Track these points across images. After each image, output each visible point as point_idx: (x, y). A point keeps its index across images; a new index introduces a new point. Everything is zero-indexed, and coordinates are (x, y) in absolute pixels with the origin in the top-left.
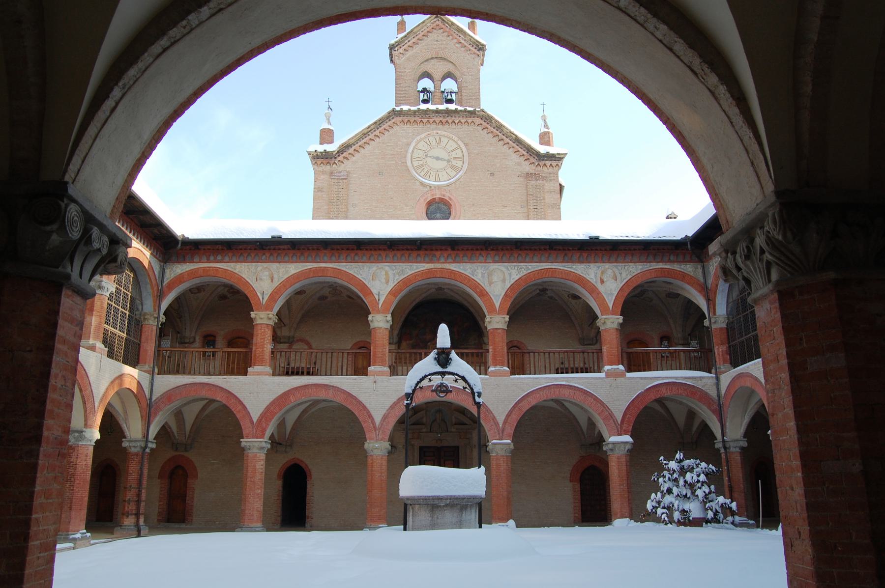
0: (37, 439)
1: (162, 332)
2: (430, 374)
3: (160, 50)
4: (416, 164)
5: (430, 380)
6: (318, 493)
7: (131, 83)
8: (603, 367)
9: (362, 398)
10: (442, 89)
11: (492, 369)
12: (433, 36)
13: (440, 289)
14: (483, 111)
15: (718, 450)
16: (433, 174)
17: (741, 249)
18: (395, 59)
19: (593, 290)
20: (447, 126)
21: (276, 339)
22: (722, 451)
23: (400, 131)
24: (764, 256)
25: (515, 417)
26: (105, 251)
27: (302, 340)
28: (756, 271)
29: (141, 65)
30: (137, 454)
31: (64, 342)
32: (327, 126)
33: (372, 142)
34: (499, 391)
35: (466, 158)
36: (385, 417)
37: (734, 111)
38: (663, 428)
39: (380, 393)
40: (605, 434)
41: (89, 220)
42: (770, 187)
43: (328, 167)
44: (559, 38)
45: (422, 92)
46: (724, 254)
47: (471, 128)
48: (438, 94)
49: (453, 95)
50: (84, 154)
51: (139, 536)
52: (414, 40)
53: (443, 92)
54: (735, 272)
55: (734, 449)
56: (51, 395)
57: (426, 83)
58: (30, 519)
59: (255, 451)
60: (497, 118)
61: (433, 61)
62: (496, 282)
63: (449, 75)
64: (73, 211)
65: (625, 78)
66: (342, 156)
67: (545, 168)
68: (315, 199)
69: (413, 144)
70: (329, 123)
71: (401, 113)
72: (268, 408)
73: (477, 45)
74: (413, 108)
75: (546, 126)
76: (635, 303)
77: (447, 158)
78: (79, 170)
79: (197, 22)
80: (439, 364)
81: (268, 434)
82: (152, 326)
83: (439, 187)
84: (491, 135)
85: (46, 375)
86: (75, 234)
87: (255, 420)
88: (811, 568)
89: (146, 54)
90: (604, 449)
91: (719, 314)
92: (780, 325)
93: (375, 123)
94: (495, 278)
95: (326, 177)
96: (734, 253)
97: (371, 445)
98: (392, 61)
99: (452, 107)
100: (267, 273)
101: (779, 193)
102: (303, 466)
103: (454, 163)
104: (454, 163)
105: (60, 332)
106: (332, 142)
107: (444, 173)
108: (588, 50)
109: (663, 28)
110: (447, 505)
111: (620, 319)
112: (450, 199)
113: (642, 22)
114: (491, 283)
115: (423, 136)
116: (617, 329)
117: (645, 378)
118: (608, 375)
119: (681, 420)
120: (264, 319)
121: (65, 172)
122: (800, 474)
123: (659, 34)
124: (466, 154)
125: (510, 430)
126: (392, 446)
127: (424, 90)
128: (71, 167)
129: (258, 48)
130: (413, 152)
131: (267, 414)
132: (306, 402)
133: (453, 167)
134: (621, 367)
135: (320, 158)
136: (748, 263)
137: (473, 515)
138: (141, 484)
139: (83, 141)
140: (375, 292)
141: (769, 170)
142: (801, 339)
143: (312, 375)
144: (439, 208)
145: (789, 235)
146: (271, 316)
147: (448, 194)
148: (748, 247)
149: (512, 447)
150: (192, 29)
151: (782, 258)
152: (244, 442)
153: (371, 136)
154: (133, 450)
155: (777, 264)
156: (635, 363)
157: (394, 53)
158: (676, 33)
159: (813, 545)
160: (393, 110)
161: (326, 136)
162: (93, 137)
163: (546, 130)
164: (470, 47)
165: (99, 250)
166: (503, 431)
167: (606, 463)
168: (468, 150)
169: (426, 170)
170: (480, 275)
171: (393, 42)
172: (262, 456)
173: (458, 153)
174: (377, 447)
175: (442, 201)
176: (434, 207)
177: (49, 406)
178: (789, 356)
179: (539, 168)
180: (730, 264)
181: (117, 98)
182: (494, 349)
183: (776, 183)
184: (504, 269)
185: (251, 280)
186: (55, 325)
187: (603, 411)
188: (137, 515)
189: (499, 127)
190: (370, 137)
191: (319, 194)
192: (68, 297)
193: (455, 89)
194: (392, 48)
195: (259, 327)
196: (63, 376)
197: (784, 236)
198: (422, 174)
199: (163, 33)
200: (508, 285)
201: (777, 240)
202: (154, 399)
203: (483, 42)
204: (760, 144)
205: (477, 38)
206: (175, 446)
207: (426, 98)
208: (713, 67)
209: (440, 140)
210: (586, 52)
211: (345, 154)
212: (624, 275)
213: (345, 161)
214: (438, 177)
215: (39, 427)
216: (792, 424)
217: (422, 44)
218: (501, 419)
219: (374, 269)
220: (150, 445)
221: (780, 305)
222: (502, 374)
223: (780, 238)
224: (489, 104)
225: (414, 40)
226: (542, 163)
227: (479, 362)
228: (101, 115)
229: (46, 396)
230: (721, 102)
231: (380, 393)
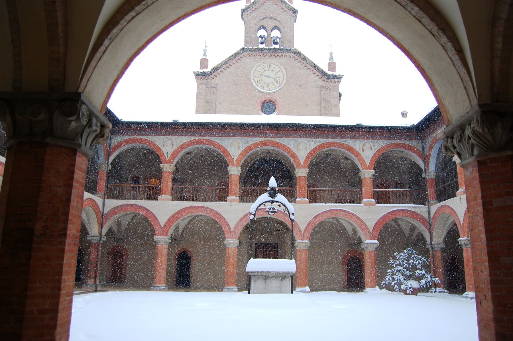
0: (65, 235)
1: (110, 175)
2: (265, 202)
3: (130, 18)
4: (256, 80)
5: (265, 205)
6: (196, 267)
7: (114, 37)
8: (362, 199)
9: (223, 214)
10: (272, 36)
11: (298, 200)
13: (269, 153)
14: (295, 49)
15: (428, 249)
16: (266, 85)
17: (456, 136)
18: (245, 18)
19: (357, 155)
20: (274, 58)
21: (174, 181)
22: (430, 249)
23: (247, 60)
24: (470, 141)
26: (98, 131)
28: (465, 149)
29: (120, 26)
30: (95, 244)
31: (78, 182)
33: (231, 67)
34: (302, 213)
35: (285, 77)
37: (456, 58)
38: (393, 236)
39: (235, 212)
40: (363, 238)
41: (91, 114)
42: (475, 102)
43: (205, 81)
44: (354, 13)
46: (446, 139)
49: (278, 39)
50: (88, 77)
51: (96, 291)
52: (255, 7)
54: (452, 149)
55: (437, 248)
56: (71, 211)
57: (262, 32)
58: (61, 279)
59: (162, 243)
62: (301, 151)
63: (276, 28)
64: (84, 110)
65: (392, 36)
66: (213, 74)
67: (331, 84)
68: (197, 99)
69: (254, 68)
72: (169, 220)
76: (382, 163)
77: (274, 77)
78: (86, 86)
79: (151, 2)
80: (270, 196)
81: (169, 234)
82: (104, 170)
83: (269, 93)
85: (69, 200)
86: (84, 122)
87: (162, 226)
88: (491, 316)
89: (123, 21)
90: (362, 247)
91: (431, 171)
92: (478, 180)
94: (301, 147)
96: (452, 138)
97: (228, 242)
98: (243, 19)
99: (277, 46)
100: (170, 142)
101: (481, 106)
103: (278, 79)
105: (76, 176)
108: (371, 20)
109: (417, 9)
110: (273, 277)
111: (373, 172)
113: (404, 5)
114: (298, 150)
115: (260, 63)
116: (371, 178)
117: (387, 207)
118: (365, 204)
119: (407, 232)
120: (168, 168)
121: (79, 87)
122: (487, 264)
123: (413, 12)
124: (285, 74)
125: (308, 235)
126: (240, 242)
127: (262, 37)
128: (82, 84)
129: (183, 16)
131: (170, 222)
132: (191, 216)
134: (373, 200)
135: (200, 76)
136: (460, 144)
137: (288, 283)
138: (97, 259)
139: (88, 70)
141: (475, 92)
142: (490, 188)
143: (195, 201)
144: (268, 106)
145: (486, 129)
146: (172, 166)
148: (461, 135)
150: (148, 6)
151: (481, 142)
152: (156, 238)
153: (230, 63)
154: (93, 241)
155: (477, 145)
156: (381, 198)
158: (424, 12)
159: (494, 303)
160: (243, 48)
161: (204, 62)
162: (94, 67)
164: (289, 11)
165: (96, 131)
167: (363, 255)
168: (286, 72)
169: (261, 84)
172: (166, 246)
174: (232, 242)
177: (70, 217)
178: (483, 197)
179: (327, 83)
180: (449, 145)
181: (106, 45)
183: (479, 99)
184: (306, 142)
185: (161, 146)
186: (73, 172)
187: (362, 225)
188: (95, 278)
189: (305, 59)
192: (80, 157)
194: (243, 11)
195: (165, 173)
196: (77, 201)
197: (483, 130)
198: (259, 86)
199: (132, 8)
201: (478, 132)
202: (105, 213)
204: (470, 77)
205: (292, 5)
206: (116, 240)
208: (444, 31)
210: (370, 21)
212: (376, 146)
213: (215, 77)
215: (65, 229)
216: (483, 236)
220: (103, 239)
221: (479, 169)
222: (304, 202)
223: (480, 131)
224: (298, 45)
225: (255, 7)
226: (329, 80)
227: (291, 196)
228: (98, 55)
229: (69, 212)
230: (448, 52)
231: (235, 212)
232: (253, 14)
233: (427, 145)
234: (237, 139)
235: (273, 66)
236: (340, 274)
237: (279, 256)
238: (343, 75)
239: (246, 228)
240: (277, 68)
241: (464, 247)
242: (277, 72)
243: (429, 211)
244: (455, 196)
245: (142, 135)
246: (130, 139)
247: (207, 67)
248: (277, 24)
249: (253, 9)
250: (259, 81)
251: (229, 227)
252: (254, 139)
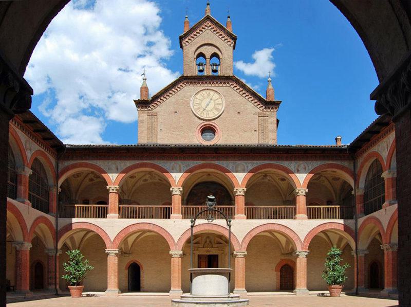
4: (195, 107)
23: (188, 89)
39: (177, 228)
91: (359, 190)
125: (245, 245)
156: (312, 215)
161: (144, 89)
170: (231, 167)
212: (310, 167)
218: (240, 240)
219: (174, 163)
233: (359, 164)
234: (179, 162)
236: (273, 277)
238: (281, 102)
239: (188, 241)
241: (386, 252)
242: (216, 100)
243: (356, 224)
244: (381, 209)
245: (87, 160)
246: (76, 164)
251: (174, 240)
252: (195, 162)
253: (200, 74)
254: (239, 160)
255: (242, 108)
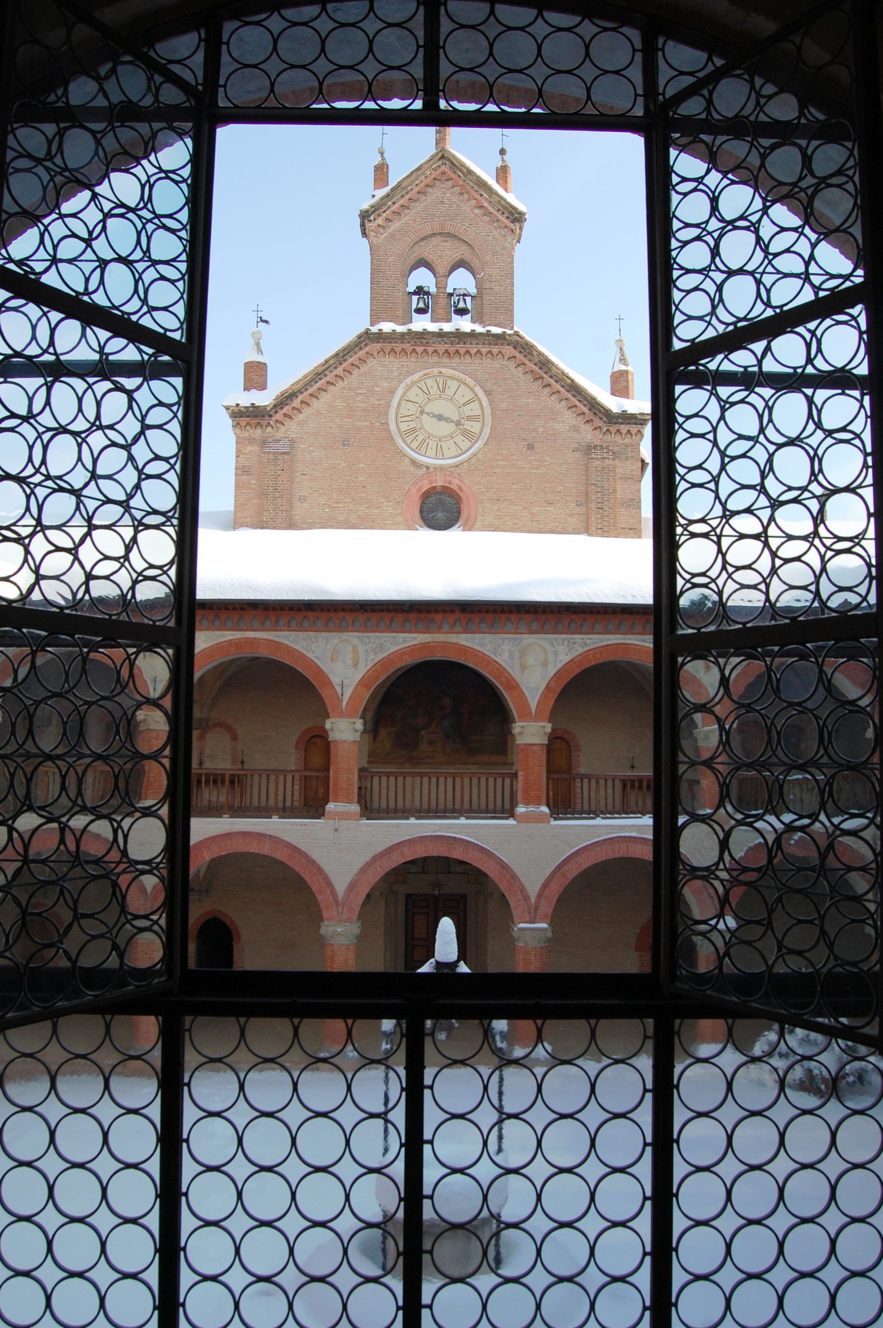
4: (404, 427)
9: (315, 855)
10: (450, 290)
11: (521, 809)
12: (435, 194)
14: (517, 334)
16: (432, 444)
20: (456, 360)
23: (379, 366)
25: (555, 890)
27: (220, 725)
32: (256, 358)
33: (331, 387)
36: (352, 886)
43: (259, 431)
45: (415, 293)
47: (497, 364)
48: (443, 301)
49: (468, 299)
53: (451, 295)
57: (422, 278)
60: (541, 348)
61: (434, 241)
63: (461, 264)
67: (618, 438)
68: (238, 487)
70: (260, 351)
71: (381, 337)
73: (510, 213)
74: (401, 329)
75: (623, 360)
77: (455, 417)
83: (442, 469)
84: (529, 376)
93: (337, 355)
94: (530, 660)
95: (256, 448)
97: (331, 929)
98: (364, 234)
102: (228, 922)
103: (468, 425)
104: (468, 425)
106: (263, 387)
107: (451, 443)
112: (460, 488)
114: (523, 668)
115: (416, 377)
124: (488, 411)
125: (547, 908)
127: (420, 291)
130: (399, 405)
133: (466, 434)
140: (335, 680)
147: (456, 481)
149: (549, 934)
153: (330, 377)
157: (367, 225)
160: (367, 332)
163: (623, 368)
166: (537, 908)
168: (491, 402)
169: (420, 438)
170: (506, 655)
171: (365, 206)
173: (474, 409)
175: (446, 491)
176: (432, 499)
179: (608, 437)
182: (526, 777)
184: (546, 645)
189: (545, 364)
190: (328, 379)
191: (245, 478)
193: (473, 291)
194: (365, 216)
198: (414, 445)
200: (552, 671)
203: (521, 207)
207: (421, 305)
209: (445, 384)
211: (286, 410)
214: (439, 453)
217: (418, 207)
219: (335, 641)
224: (526, 325)
225: (402, 202)
226: (613, 429)
232: (395, 225)
235: (453, 385)
237: (478, 524)
240: (463, 389)
242: (465, 405)
247: (263, 387)
248: (468, 256)
249: (394, 208)
250: (414, 430)
253: (194, 780)
254: (531, 632)
255: (540, 430)
